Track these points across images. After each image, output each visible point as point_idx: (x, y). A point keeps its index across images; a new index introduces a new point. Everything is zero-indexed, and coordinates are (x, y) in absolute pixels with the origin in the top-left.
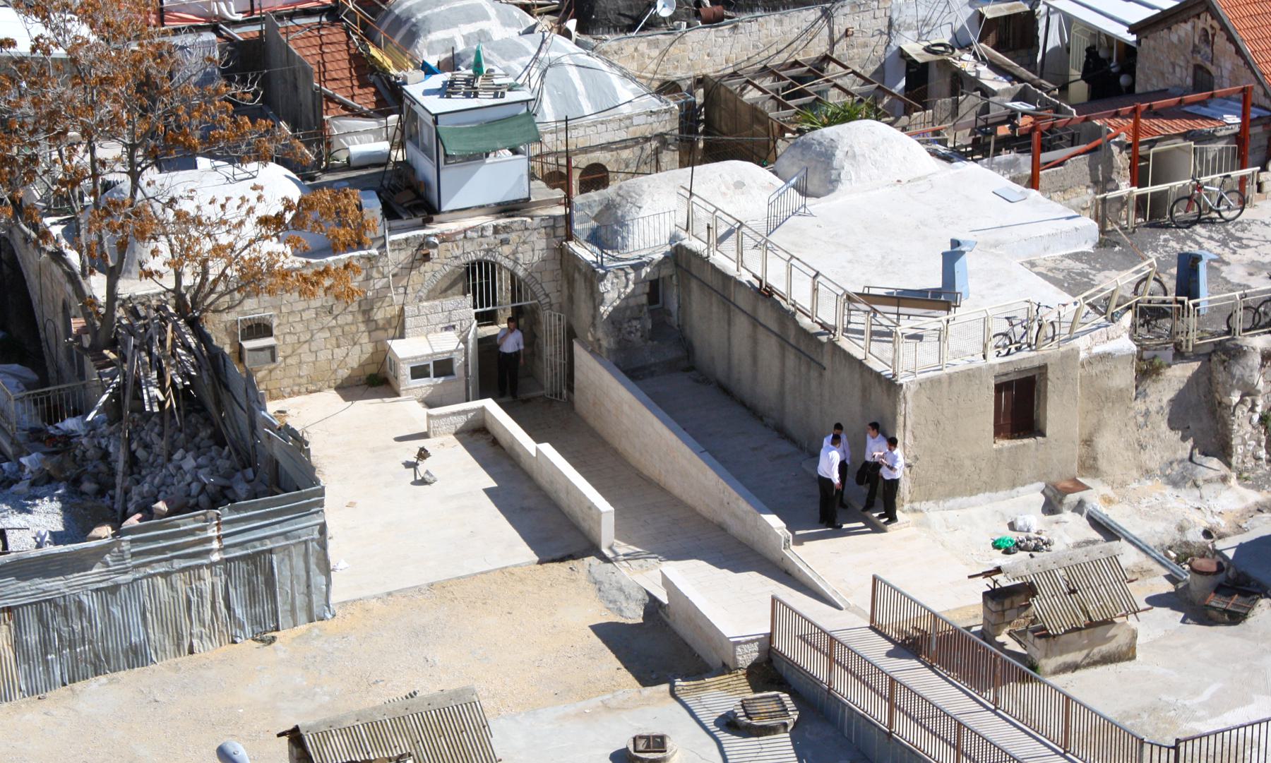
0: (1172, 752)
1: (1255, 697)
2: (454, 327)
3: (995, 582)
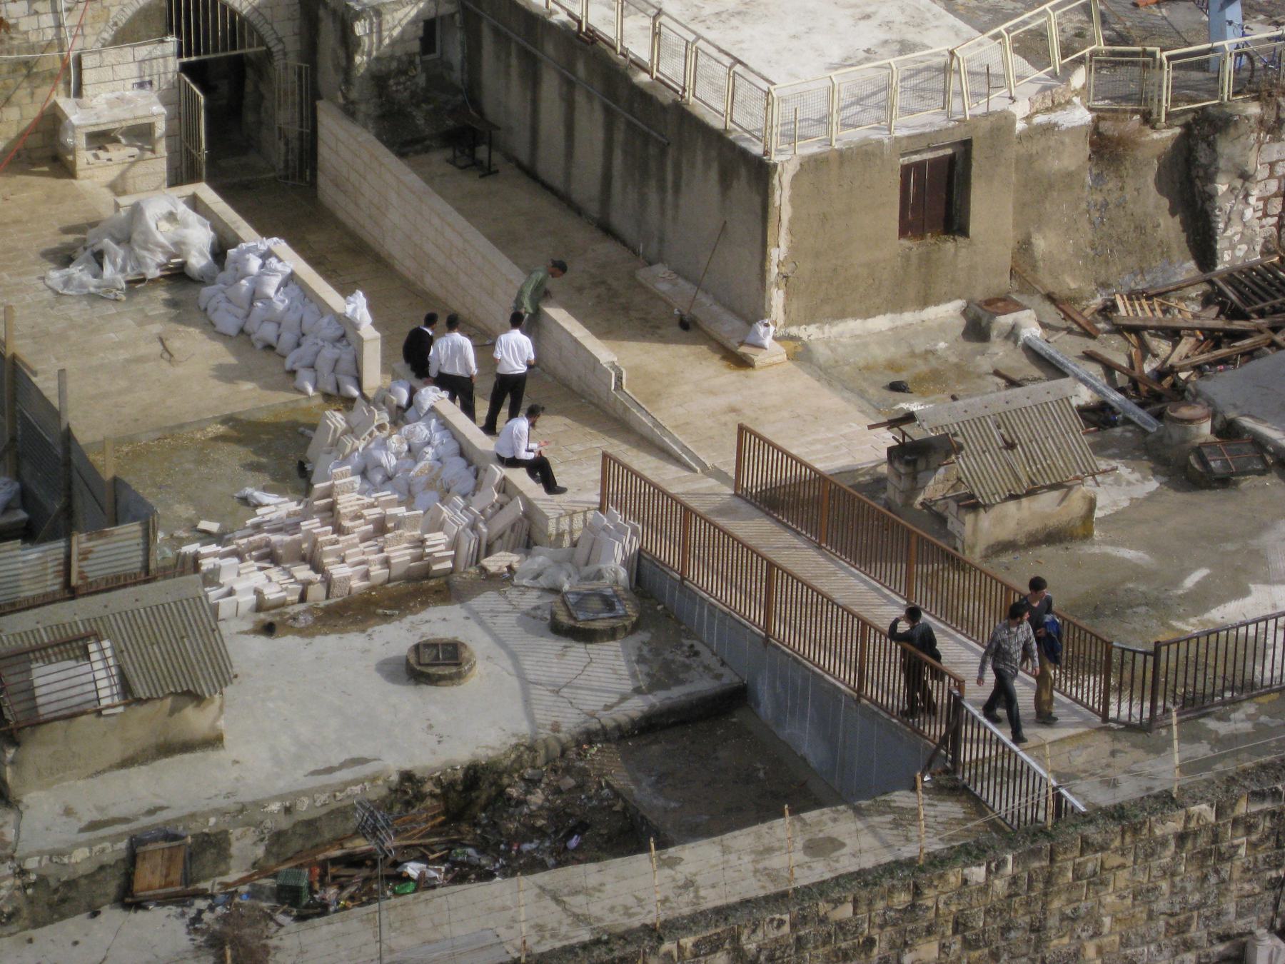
0: (1150, 659)
1: (1252, 587)
2: (151, 83)
3: (904, 434)
